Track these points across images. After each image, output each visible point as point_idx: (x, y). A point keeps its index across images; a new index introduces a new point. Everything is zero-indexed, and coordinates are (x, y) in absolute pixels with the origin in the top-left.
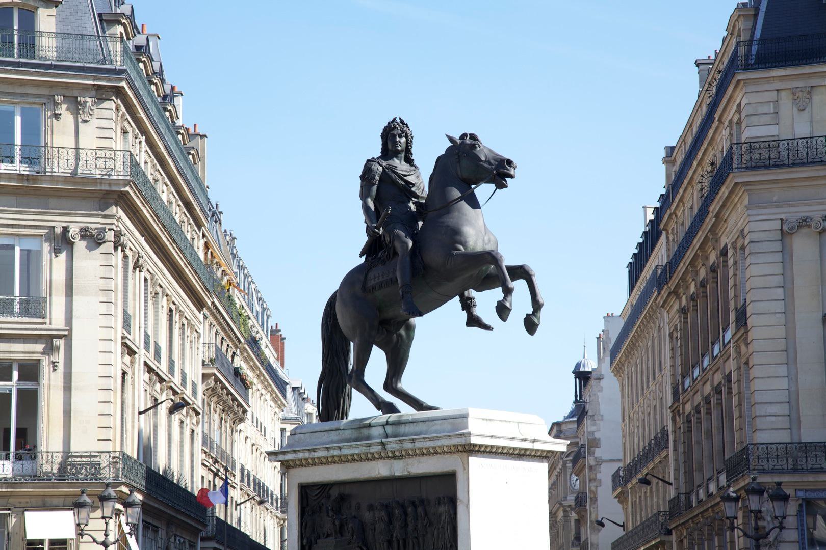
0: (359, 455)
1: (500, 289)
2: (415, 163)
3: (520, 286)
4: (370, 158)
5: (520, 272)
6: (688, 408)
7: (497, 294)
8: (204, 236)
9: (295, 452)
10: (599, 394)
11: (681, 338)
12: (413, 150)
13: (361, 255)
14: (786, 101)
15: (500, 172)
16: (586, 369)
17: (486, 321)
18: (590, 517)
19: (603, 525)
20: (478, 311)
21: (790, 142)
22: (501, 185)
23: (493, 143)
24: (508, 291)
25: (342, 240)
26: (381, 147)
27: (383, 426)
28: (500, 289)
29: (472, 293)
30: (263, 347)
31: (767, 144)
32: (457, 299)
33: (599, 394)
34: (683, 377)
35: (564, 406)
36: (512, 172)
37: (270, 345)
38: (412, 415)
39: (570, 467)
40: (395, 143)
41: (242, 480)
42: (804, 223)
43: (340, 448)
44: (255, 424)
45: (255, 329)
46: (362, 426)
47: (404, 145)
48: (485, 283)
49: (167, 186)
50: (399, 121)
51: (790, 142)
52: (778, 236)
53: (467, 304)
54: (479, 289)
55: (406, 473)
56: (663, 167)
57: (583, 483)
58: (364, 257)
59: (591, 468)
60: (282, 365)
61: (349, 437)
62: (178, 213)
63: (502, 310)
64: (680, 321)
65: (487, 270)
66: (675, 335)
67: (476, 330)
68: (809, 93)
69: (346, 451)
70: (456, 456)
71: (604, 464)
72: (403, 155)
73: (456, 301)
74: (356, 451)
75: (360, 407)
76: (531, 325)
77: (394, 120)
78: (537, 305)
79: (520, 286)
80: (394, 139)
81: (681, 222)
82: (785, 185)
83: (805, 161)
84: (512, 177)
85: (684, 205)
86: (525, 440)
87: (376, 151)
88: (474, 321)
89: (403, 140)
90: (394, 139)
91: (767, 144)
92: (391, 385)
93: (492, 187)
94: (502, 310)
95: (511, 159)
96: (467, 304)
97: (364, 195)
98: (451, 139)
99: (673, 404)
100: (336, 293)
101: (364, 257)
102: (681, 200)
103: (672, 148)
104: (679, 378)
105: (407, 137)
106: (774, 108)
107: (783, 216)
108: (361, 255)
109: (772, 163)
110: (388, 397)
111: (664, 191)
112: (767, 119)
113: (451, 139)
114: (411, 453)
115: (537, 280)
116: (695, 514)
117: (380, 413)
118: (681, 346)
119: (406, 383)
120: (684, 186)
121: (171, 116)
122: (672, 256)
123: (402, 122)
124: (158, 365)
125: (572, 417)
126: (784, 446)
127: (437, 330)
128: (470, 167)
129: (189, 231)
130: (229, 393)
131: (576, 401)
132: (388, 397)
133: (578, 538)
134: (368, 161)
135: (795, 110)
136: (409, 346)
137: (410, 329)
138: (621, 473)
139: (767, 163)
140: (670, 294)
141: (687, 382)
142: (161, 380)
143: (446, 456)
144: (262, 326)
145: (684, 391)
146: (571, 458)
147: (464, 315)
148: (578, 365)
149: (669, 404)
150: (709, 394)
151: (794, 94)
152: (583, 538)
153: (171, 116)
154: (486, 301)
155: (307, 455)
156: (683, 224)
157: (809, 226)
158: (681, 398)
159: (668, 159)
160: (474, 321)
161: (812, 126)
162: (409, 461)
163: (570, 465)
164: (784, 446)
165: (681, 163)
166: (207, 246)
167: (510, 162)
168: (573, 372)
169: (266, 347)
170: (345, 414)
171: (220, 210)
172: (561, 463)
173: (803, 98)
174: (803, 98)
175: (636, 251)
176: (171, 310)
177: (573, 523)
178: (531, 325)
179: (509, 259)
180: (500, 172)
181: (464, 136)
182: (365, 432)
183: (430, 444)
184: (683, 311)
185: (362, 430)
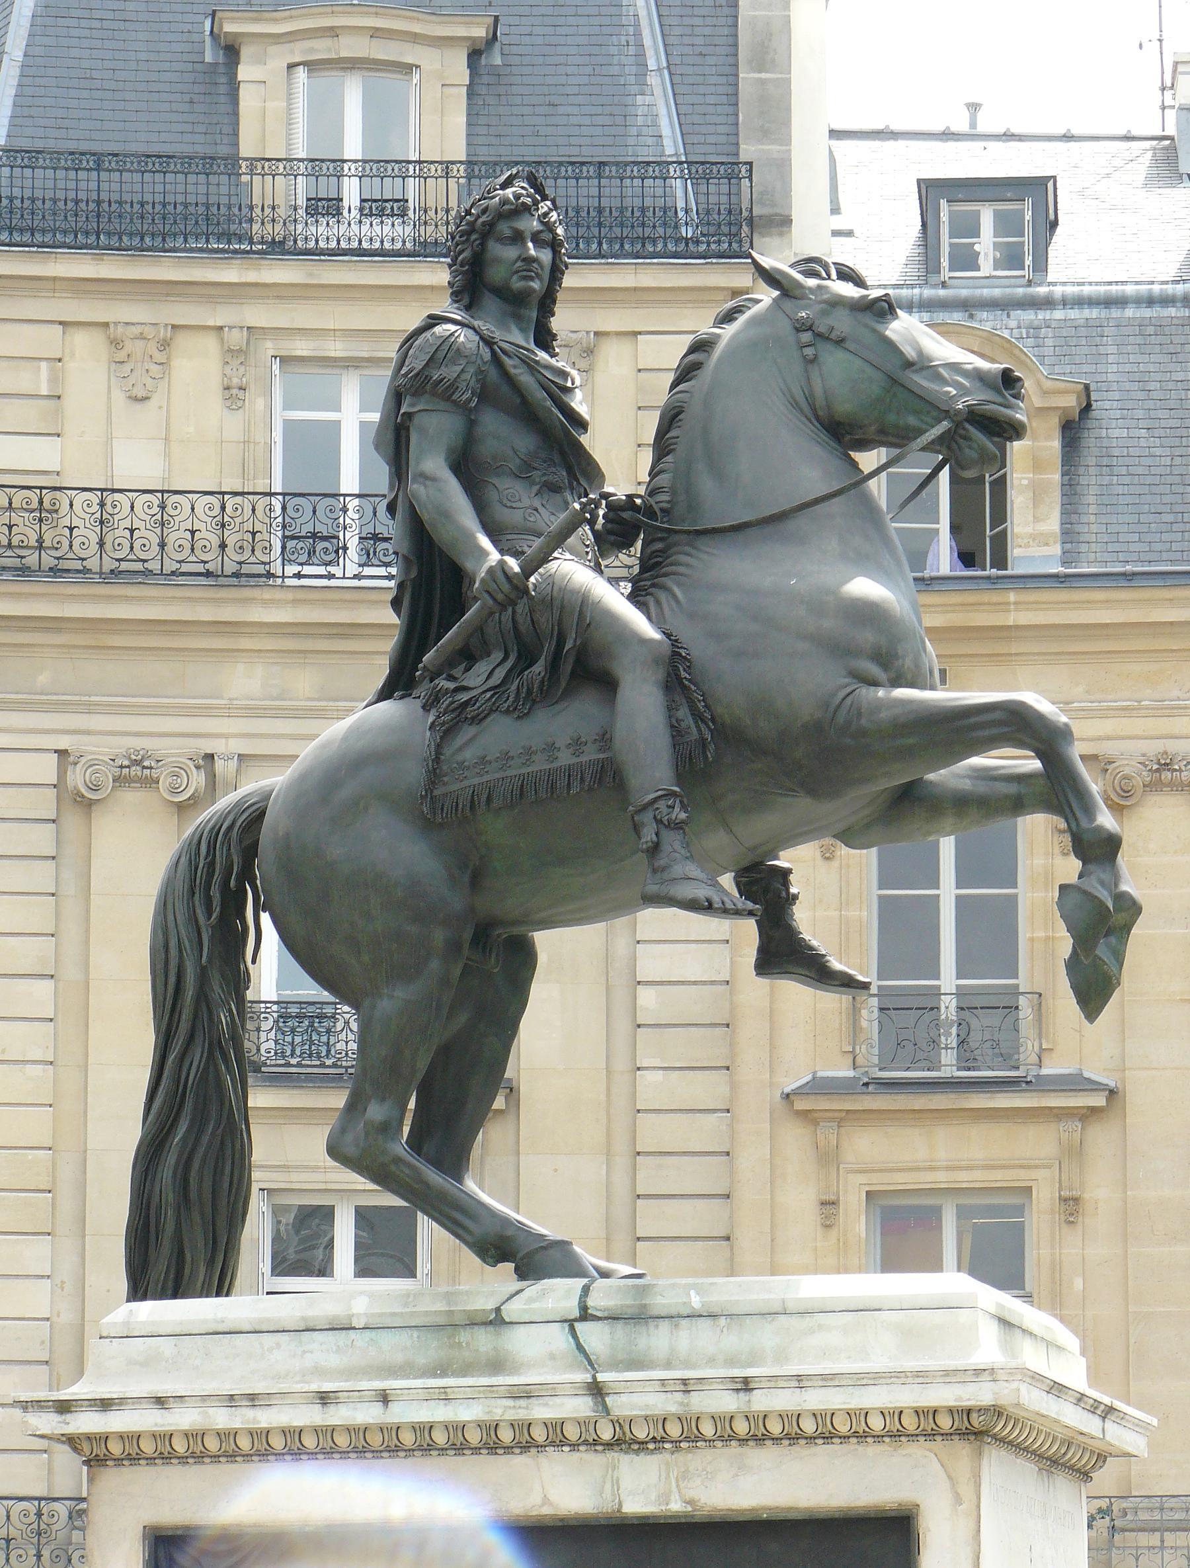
9: (160, 1402)
14: (86, 359)
20: (810, 921)
21: (230, 502)
27: (571, 1323)
31: (34, 496)
42: (136, 772)
43: (384, 1398)
51: (230, 502)
52: (46, 804)
55: (676, 1506)
61: (399, 1358)
65: (882, 765)
68: (165, 345)
69: (405, 1413)
70: (919, 1451)
74: (468, 1413)
82: (80, 640)
83: (154, 566)
91: (34, 496)
96: (767, 894)
106: (54, 379)
107: (63, 743)
109: (48, 561)
112: (27, 414)
126: (31, 1507)
135: (119, 397)
137: (522, 959)
139: (32, 559)
143: (872, 1450)
151: (116, 343)
155: (222, 1419)
157: (151, 783)
161: (167, 455)
162: (698, 1459)
164: (31, 1507)
173: (140, 364)
174: (140, 364)
182: (483, 1341)
183: (815, 1399)
185: (464, 1336)
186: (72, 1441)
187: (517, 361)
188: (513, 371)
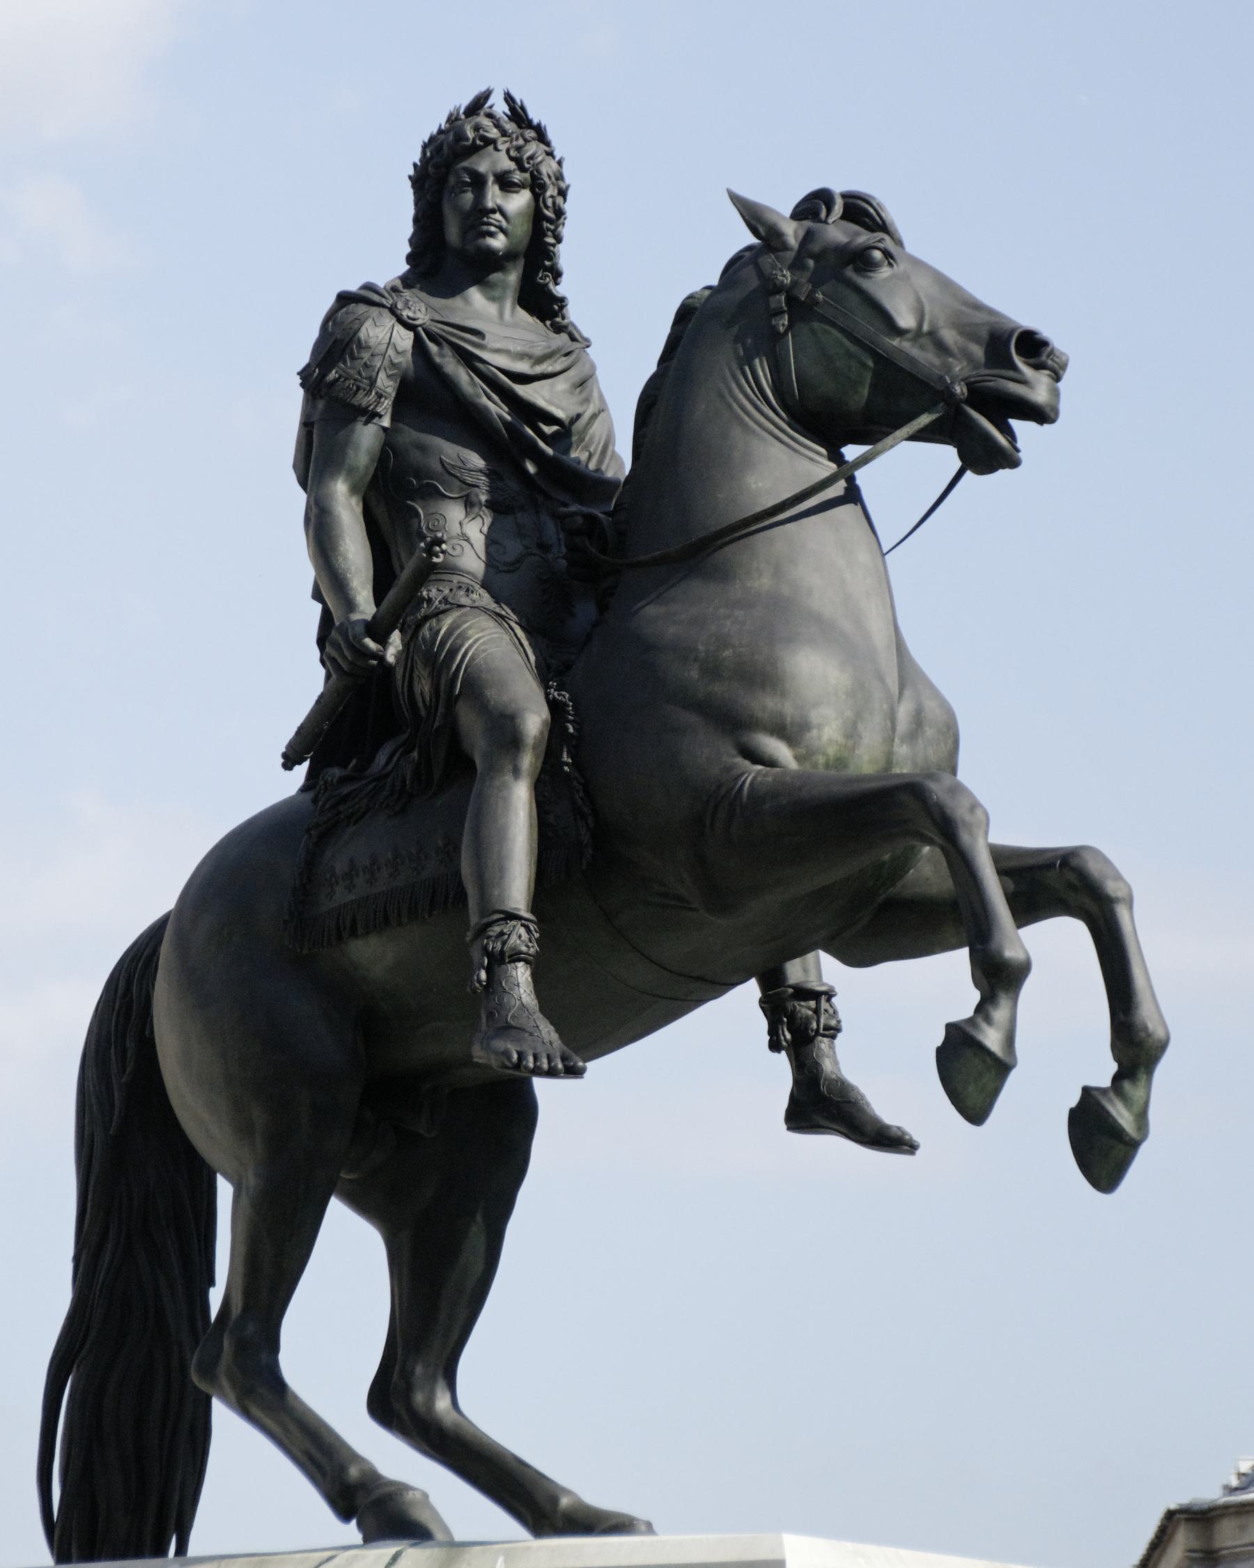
2: (575, 314)
3: (1057, 949)
4: (353, 286)
5: (1059, 883)
12: (566, 255)
13: (290, 761)
15: (982, 395)
17: (886, 1108)
20: (850, 1060)
22: (985, 457)
23: (963, 246)
24: (999, 977)
26: (409, 229)
29: (828, 969)
32: (750, 991)
47: (522, 230)
48: (887, 926)
50: (499, 107)
53: (797, 1025)
54: (859, 953)
58: (302, 770)
63: (971, 1070)
67: (831, 1148)
72: (513, 277)
77: (477, 105)
78: (1135, 1049)
79: (1057, 949)
84: (1041, 415)
87: (384, 254)
88: (821, 1105)
90: (478, 204)
93: (946, 457)
94: (971, 1070)
96: (797, 1025)
97: (316, 458)
98: (752, 215)
100: (154, 935)
101: (302, 770)
108: (290, 761)
113: (752, 215)
115: (1146, 929)
119: (490, 1388)
123: (518, 115)
127: (647, 1131)
128: (845, 343)
134: (344, 299)
137: (523, 1115)
147: (780, 1070)
154: (890, 1011)
167: (1033, 346)
178: (1101, 1143)
180: (982, 395)
181: (814, 206)
187: (447, 351)
188: (438, 360)
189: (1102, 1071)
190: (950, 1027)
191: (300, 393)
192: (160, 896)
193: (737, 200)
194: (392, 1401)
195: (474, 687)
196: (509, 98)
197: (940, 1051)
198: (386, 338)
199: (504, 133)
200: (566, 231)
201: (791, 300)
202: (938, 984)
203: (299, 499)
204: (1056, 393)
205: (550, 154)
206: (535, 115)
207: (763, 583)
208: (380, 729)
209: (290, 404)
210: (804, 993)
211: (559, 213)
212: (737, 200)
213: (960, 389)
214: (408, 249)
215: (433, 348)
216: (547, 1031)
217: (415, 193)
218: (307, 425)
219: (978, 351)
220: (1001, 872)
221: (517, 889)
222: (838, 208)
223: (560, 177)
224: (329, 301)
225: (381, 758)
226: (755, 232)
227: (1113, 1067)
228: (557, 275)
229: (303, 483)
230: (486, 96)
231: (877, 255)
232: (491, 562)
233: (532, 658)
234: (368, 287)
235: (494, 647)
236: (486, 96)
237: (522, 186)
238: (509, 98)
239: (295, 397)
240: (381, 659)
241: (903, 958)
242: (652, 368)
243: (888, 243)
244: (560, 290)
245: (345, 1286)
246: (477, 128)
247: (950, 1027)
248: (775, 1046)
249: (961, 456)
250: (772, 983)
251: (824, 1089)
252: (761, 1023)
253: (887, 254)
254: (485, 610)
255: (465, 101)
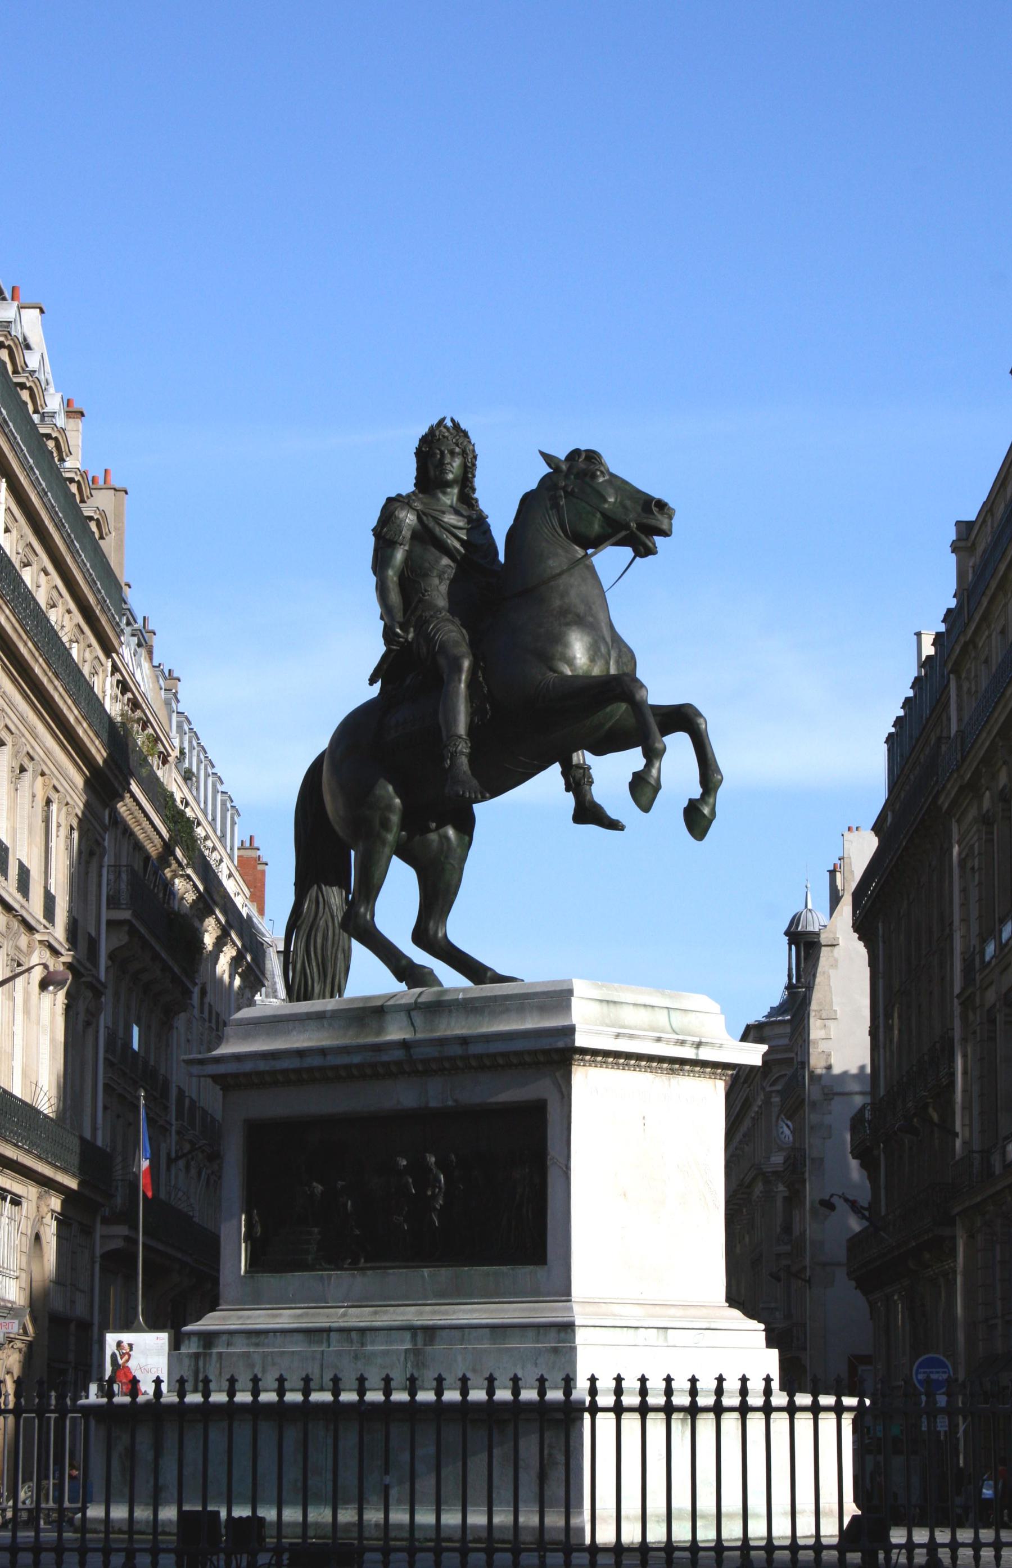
0: (359, 1066)
1: (639, 750)
3: (678, 747)
4: (393, 495)
5: (682, 718)
6: (991, 996)
7: (633, 759)
8: (115, 669)
10: (832, 972)
11: (980, 869)
12: (478, 482)
13: (372, 681)
15: (641, 523)
16: (810, 929)
17: (612, 813)
18: (811, 1193)
19: (832, 1207)
22: (644, 550)
23: (633, 462)
24: (653, 754)
25: (340, 662)
26: (415, 474)
28: (639, 750)
29: (589, 758)
30: (223, 877)
32: (556, 768)
33: (832, 972)
34: (984, 941)
35: (769, 991)
36: (665, 527)
37: (236, 874)
38: (464, 990)
39: (769, 1101)
40: (441, 465)
41: (180, 1116)
44: (206, 1015)
45: (209, 843)
46: (373, 1012)
49: (47, 574)
50: (449, 424)
53: (577, 782)
54: (600, 749)
56: (953, 558)
57: (798, 1132)
59: (813, 1105)
60: (261, 911)
62: (64, 619)
63: (643, 789)
64: (979, 839)
65: (617, 713)
66: (969, 865)
71: (625, 1554)
72: (456, 491)
73: (556, 768)
75: (367, 977)
76: (697, 819)
77: (441, 422)
79: (678, 747)
80: (442, 457)
81: (983, 658)
84: (666, 534)
85: (989, 626)
86: (683, 1043)
87: (405, 483)
88: (587, 813)
89: (457, 463)
90: (442, 457)
92: (428, 932)
93: (628, 552)
94: (643, 789)
95: (666, 499)
96: (577, 782)
97: (380, 563)
98: (548, 458)
99: (963, 989)
100: (322, 756)
101: (378, 686)
102: (985, 618)
103: (969, 525)
104: (975, 941)
105: (464, 453)
108: (372, 681)
110: (420, 957)
111: (953, 603)
113: (548, 458)
114: (460, 1064)
116: (998, 1188)
117: (403, 987)
118: (980, 884)
119: (460, 928)
120: (990, 593)
121: (58, 446)
122: (966, 718)
123: (456, 426)
124: (23, 901)
125: (782, 1014)
127: (521, 821)
129: (83, 652)
130: (156, 957)
131: (789, 987)
132: (420, 957)
133: (787, 1228)
134: (390, 500)
136: (463, 859)
137: (466, 825)
138: (867, 1115)
140: (962, 789)
141: (990, 949)
142: (31, 929)
144: (222, 838)
145: (985, 965)
146: (778, 1087)
147: (569, 800)
148: (795, 920)
149: (957, 990)
150: (994, 1005)
152: (796, 1231)
153: (58, 446)
154: (611, 772)
156: (986, 661)
158: (978, 977)
159: (962, 544)
160: (587, 813)
163: (776, 1099)
165: (985, 551)
166: (124, 686)
167: (661, 505)
168: (786, 933)
169: (230, 875)
170: (337, 988)
171: (151, 627)
172: (762, 1096)
175: (901, 713)
176: (48, 802)
177: (779, 1203)
178: (697, 819)
179: (659, 691)
180: (641, 523)
181: (574, 454)
184: (986, 820)
186: (216, 1078)
189: (697, 792)
190: (634, 774)
191: (373, 539)
192: (322, 743)
193: (542, 454)
194: (422, 936)
195: (443, 648)
196: (452, 420)
197: (631, 784)
198: (409, 518)
199: (451, 434)
200: (477, 473)
201: (565, 492)
202: (631, 760)
203: (373, 580)
204: (671, 525)
205: (470, 442)
206: (463, 426)
207: (557, 603)
208: (406, 668)
209: (369, 542)
210: (579, 766)
211: (474, 465)
212: (542, 454)
213: (633, 525)
214: (414, 481)
215: (425, 518)
216: (475, 782)
217: (417, 462)
218: (376, 550)
219: (639, 509)
220: (654, 715)
221: (462, 729)
222: (583, 456)
223: (474, 451)
224: (383, 502)
225: (408, 681)
226: (551, 467)
227: (701, 790)
228: (474, 490)
229: (375, 573)
230: (444, 419)
231: (598, 473)
232: (450, 601)
233: (467, 637)
234: (399, 495)
235: (452, 633)
236: (444, 419)
237: (458, 454)
238: (452, 420)
239: (371, 540)
240: (406, 640)
241: (726, 1214)
242: (512, 522)
243: (602, 469)
244: (476, 496)
245: (397, 900)
246: (440, 431)
247: (634, 774)
248: (567, 790)
249: (634, 551)
250: (568, 771)
251: (587, 804)
252: (561, 781)
253: (602, 472)
254: (447, 620)
255: (435, 422)
